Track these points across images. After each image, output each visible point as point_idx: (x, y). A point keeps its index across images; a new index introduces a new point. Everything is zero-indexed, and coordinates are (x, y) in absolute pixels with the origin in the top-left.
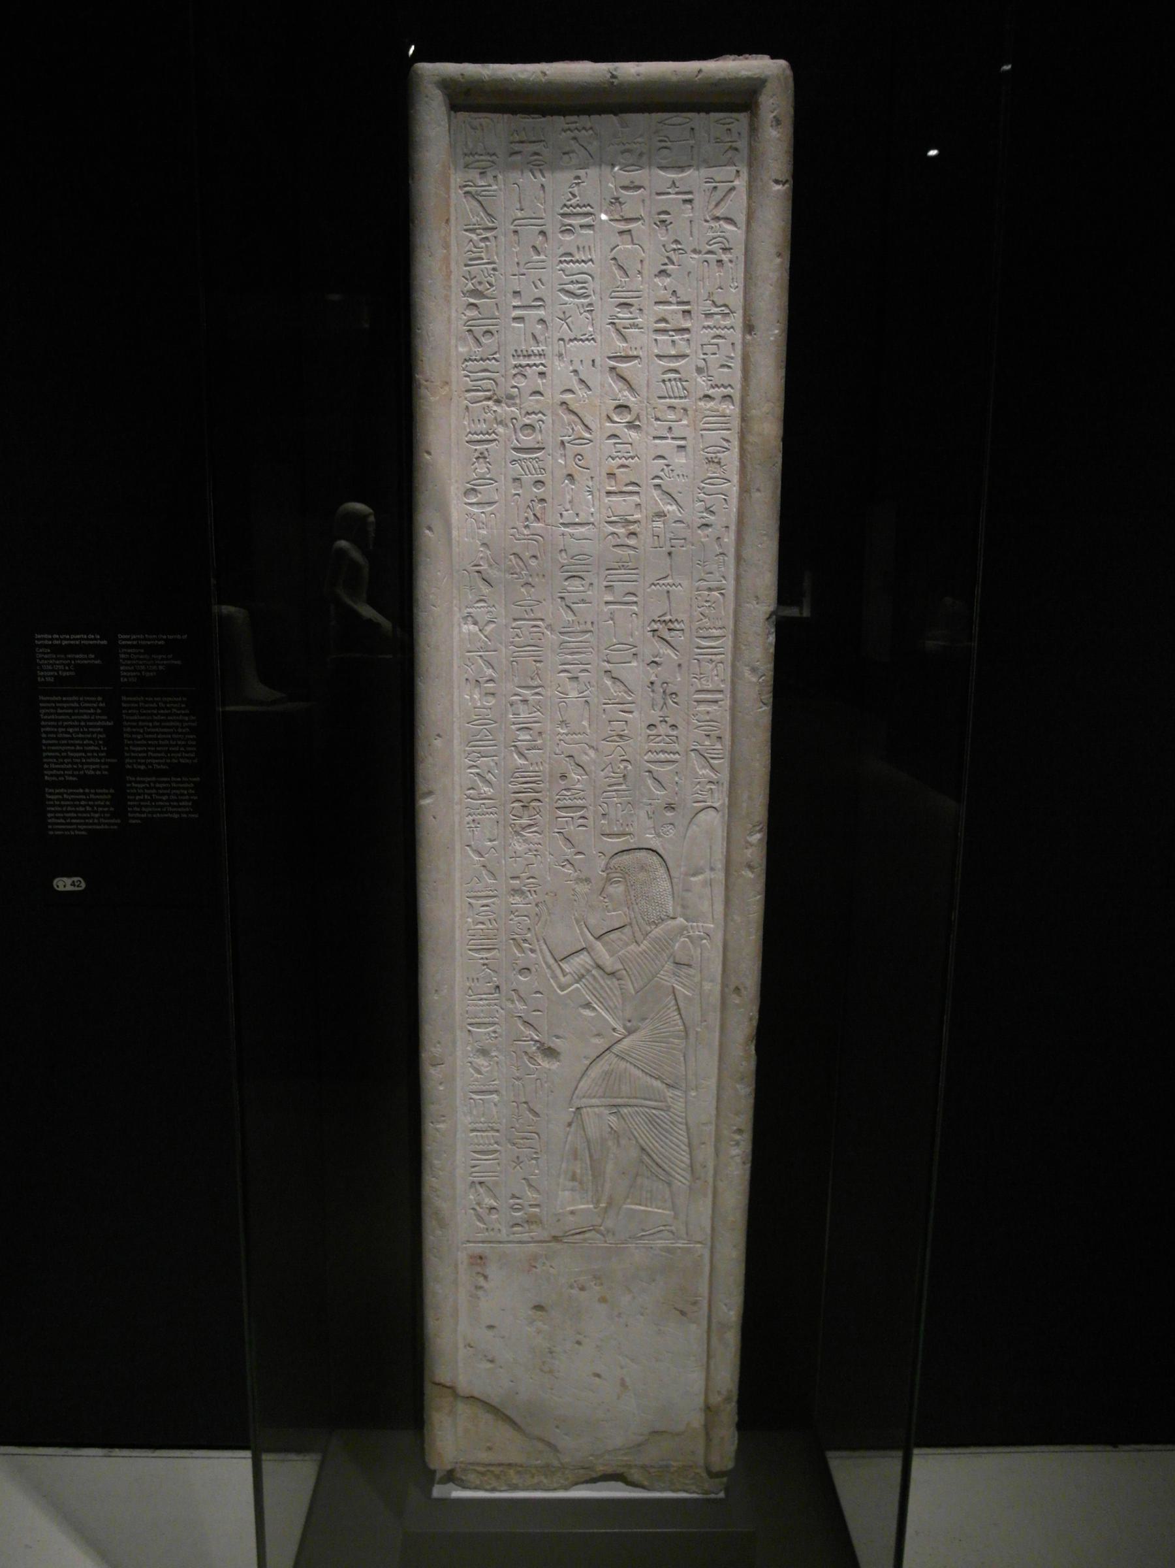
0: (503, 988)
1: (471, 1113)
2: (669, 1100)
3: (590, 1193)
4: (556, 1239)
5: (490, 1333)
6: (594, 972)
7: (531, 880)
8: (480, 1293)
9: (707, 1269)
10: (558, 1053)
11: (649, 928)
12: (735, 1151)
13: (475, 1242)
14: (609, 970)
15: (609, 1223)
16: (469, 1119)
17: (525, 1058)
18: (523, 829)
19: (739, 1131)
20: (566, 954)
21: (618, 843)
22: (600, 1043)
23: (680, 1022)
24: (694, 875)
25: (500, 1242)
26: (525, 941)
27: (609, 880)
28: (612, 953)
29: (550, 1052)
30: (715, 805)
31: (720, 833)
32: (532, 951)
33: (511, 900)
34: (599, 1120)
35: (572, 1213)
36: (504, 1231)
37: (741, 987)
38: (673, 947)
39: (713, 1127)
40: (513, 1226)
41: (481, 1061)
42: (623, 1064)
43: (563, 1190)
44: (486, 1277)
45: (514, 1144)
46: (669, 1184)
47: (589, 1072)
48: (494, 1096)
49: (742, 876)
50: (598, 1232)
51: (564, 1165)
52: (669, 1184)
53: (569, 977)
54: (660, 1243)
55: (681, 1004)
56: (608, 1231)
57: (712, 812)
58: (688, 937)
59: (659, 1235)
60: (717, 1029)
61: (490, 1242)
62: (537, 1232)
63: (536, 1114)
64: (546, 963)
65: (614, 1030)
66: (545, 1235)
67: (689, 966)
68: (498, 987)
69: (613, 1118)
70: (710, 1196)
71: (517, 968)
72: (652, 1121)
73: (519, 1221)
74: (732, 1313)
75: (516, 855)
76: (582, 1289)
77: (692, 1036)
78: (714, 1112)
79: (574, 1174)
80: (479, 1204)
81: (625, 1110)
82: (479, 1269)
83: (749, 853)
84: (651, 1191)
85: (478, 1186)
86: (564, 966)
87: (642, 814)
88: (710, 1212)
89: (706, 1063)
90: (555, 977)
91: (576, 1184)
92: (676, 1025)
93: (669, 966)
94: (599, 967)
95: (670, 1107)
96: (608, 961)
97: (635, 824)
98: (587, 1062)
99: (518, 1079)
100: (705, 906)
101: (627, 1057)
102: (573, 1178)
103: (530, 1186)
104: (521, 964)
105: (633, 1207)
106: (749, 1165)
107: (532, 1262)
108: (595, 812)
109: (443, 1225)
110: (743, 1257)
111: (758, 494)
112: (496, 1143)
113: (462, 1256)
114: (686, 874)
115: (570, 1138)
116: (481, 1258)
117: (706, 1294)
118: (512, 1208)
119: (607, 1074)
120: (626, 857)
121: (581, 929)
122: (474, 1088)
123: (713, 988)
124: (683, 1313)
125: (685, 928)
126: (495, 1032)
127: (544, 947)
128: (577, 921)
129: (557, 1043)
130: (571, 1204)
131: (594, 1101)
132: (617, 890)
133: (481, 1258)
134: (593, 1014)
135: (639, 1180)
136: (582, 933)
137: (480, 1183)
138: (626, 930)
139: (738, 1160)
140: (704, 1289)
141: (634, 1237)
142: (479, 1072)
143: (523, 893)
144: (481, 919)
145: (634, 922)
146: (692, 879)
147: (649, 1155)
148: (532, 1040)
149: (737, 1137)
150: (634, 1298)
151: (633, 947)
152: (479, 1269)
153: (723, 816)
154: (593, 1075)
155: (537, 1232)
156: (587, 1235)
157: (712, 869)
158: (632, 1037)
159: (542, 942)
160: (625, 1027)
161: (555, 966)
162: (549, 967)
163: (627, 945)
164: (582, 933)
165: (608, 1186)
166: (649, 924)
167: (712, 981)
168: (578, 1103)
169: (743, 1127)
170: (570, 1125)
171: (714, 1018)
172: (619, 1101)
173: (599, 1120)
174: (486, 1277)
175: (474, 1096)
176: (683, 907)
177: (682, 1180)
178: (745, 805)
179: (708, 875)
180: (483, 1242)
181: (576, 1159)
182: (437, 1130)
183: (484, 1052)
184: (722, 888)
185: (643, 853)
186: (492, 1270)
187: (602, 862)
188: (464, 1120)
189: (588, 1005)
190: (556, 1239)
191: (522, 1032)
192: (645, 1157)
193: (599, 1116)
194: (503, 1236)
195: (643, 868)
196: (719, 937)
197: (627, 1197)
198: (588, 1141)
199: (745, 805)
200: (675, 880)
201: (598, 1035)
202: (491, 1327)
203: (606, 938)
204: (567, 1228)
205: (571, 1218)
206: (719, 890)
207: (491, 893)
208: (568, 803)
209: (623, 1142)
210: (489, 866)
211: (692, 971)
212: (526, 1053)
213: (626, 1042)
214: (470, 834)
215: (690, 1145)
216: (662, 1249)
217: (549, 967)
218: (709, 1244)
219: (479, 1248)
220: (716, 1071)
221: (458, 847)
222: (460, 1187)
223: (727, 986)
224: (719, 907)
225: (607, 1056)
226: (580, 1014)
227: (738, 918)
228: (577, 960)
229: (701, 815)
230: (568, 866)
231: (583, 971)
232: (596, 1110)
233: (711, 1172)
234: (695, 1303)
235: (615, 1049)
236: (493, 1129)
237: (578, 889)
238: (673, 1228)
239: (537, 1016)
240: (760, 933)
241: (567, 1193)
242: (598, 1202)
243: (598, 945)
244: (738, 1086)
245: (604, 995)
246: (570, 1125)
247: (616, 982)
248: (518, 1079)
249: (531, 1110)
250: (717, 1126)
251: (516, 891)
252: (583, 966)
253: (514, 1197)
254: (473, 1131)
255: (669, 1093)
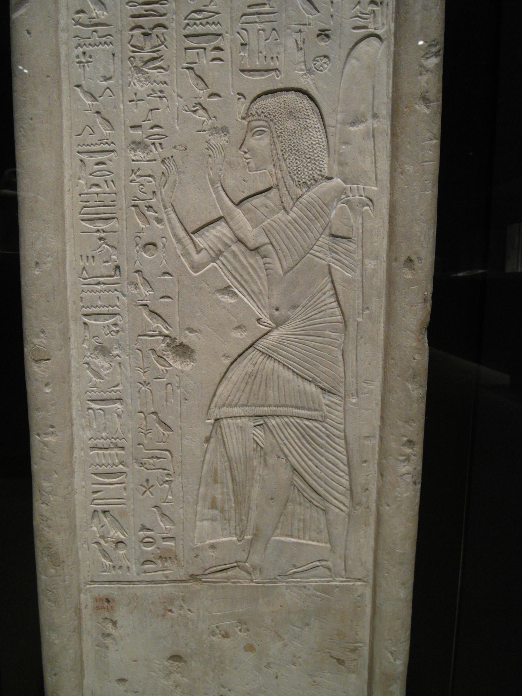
0: (125, 267)
1: (90, 426)
2: (325, 408)
3: (233, 523)
4: (194, 577)
5: (121, 688)
6: (234, 248)
7: (156, 130)
8: (108, 641)
9: (368, 610)
10: (193, 351)
11: (299, 192)
12: (404, 468)
13: (101, 582)
14: (252, 244)
15: (255, 559)
16: (89, 434)
17: (153, 357)
18: (146, 63)
19: (410, 443)
20: (200, 224)
21: (262, 82)
22: (243, 338)
23: (337, 311)
24: (353, 124)
25: (130, 582)
26: (149, 207)
27: (251, 131)
28: (255, 223)
29: (183, 350)
30: (378, 32)
31: (385, 69)
32: (159, 221)
33: (132, 155)
34: (241, 434)
35: (213, 546)
36: (134, 568)
37: (414, 257)
38: (328, 215)
39: (376, 442)
40: (143, 564)
41: (100, 362)
42: (270, 364)
43: (202, 520)
44: (114, 623)
45: (142, 464)
46: (325, 511)
47: (229, 375)
48: (118, 405)
49: (415, 111)
50: (243, 569)
51: (202, 490)
52: (325, 511)
53: (203, 253)
54: (314, 582)
55: (339, 287)
56: (254, 569)
57: (374, 41)
58: (347, 202)
59: (313, 572)
60: (382, 319)
61: (119, 582)
62: (174, 571)
63: (168, 427)
64: (175, 236)
65: (259, 320)
66: (182, 574)
67: (348, 238)
68: (118, 267)
69: (259, 432)
70: (373, 526)
71: (142, 243)
72: (305, 435)
73: (151, 557)
74: (398, 662)
75: (136, 100)
76: (226, 635)
77: (352, 327)
78: (377, 423)
79: (214, 500)
80: (103, 537)
81: (272, 422)
82: (107, 614)
83: (424, 79)
84: (304, 520)
85: (101, 515)
86: (197, 239)
87: (290, 43)
88: (372, 543)
89: (369, 361)
90: (187, 254)
91: (217, 512)
92: (333, 314)
93: (325, 240)
94: (240, 240)
95: (326, 417)
96: (252, 234)
97: (282, 57)
98: (227, 362)
99: (145, 383)
100: (367, 164)
101: (274, 355)
102: (213, 506)
103: (163, 515)
104: (146, 238)
105: (283, 539)
106: (419, 486)
107: (167, 605)
108: (233, 41)
109: (56, 561)
110: (410, 597)
111: (290, 507)
112: (121, 463)
113: (86, 599)
114: (344, 123)
115: (208, 456)
116: (108, 601)
117: (367, 640)
118: (142, 541)
119: (252, 376)
120: (270, 101)
121: (217, 192)
122: (94, 396)
123: (376, 267)
124: (340, 662)
125: (343, 191)
126: (115, 325)
127: (173, 215)
128: (213, 183)
129: (190, 339)
130: (211, 536)
131: (237, 411)
132: (260, 143)
133: (108, 601)
134: (233, 301)
135: (290, 507)
136: (219, 199)
137: (104, 512)
138: (272, 194)
139: (409, 479)
140: (365, 635)
141: (284, 575)
142: (97, 374)
143: (146, 146)
144: (96, 180)
145: (281, 183)
146: (352, 129)
147: (303, 478)
148: (161, 334)
149: (408, 450)
150: (285, 645)
151: (281, 215)
152: (107, 614)
153: (389, 47)
154: (234, 378)
155: (174, 571)
156: (230, 573)
157: (375, 116)
158: (282, 330)
159: (170, 209)
160: (272, 317)
161: (186, 240)
162: (179, 241)
163: (273, 212)
164: (219, 199)
165: (253, 514)
166: (299, 185)
167: (376, 258)
168: (216, 413)
169: (414, 438)
170: (208, 440)
171: (378, 306)
172: (265, 410)
173: (241, 434)
174: (114, 623)
175: (93, 405)
176: (341, 164)
177: (339, 505)
178: (418, 17)
179: (370, 123)
180: (110, 582)
181: (216, 482)
182: (45, 444)
183: (103, 350)
184: (388, 139)
185: (292, 95)
186: (121, 614)
187: (242, 107)
188: (83, 435)
189: (227, 290)
190: (194, 577)
191: (148, 324)
192: (296, 479)
193: (241, 428)
194: (132, 575)
195: (291, 114)
196: (383, 203)
197: (276, 528)
198: (229, 460)
199: (418, 17)
200: (330, 130)
201: (239, 327)
202: (122, 680)
203: (247, 204)
204: (207, 565)
205: (211, 553)
206: (384, 143)
207: (107, 147)
208: (200, 29)
209: (271, 460)
210: (103, 112)
211: (352, 246)
212: (153, 350)
213: (273, 336)
214: (81, 70)
215: (349, 465)
216: (316, 588)
217: (179, 241)
218: (371, 581)
219: (106, 590)
220: (381, 371)
221: (65, 86)
222: (81, 516)
223: (396, 259)
224: (384, 165)
225: (252, 354)
226: (218, 301)
227: (409, 168)
228: (214, 232)
229: (361, 45)
230: (201, 112)
231: (220, 246)
232: (239, 421)
233: (374, 496)
234: (354, 650)
235: (259, 346)
236: (117, 446)
237: (213, 142)
238: (329, 564)
239: (164, 304)
240: (436, 190)
241: (206, 523)
242: (243, 533)
243: (238, 213)
244: (410, 386)
245: (246, 277)
246: (208, 440)
247: (261, 262)
248: (145, 383)
249: (162, 423)
250: (381, 438)
251: (137, 145)
252: (220, 239)
253: (144, 528)
254: (93, 448)
255: (325, 399)
